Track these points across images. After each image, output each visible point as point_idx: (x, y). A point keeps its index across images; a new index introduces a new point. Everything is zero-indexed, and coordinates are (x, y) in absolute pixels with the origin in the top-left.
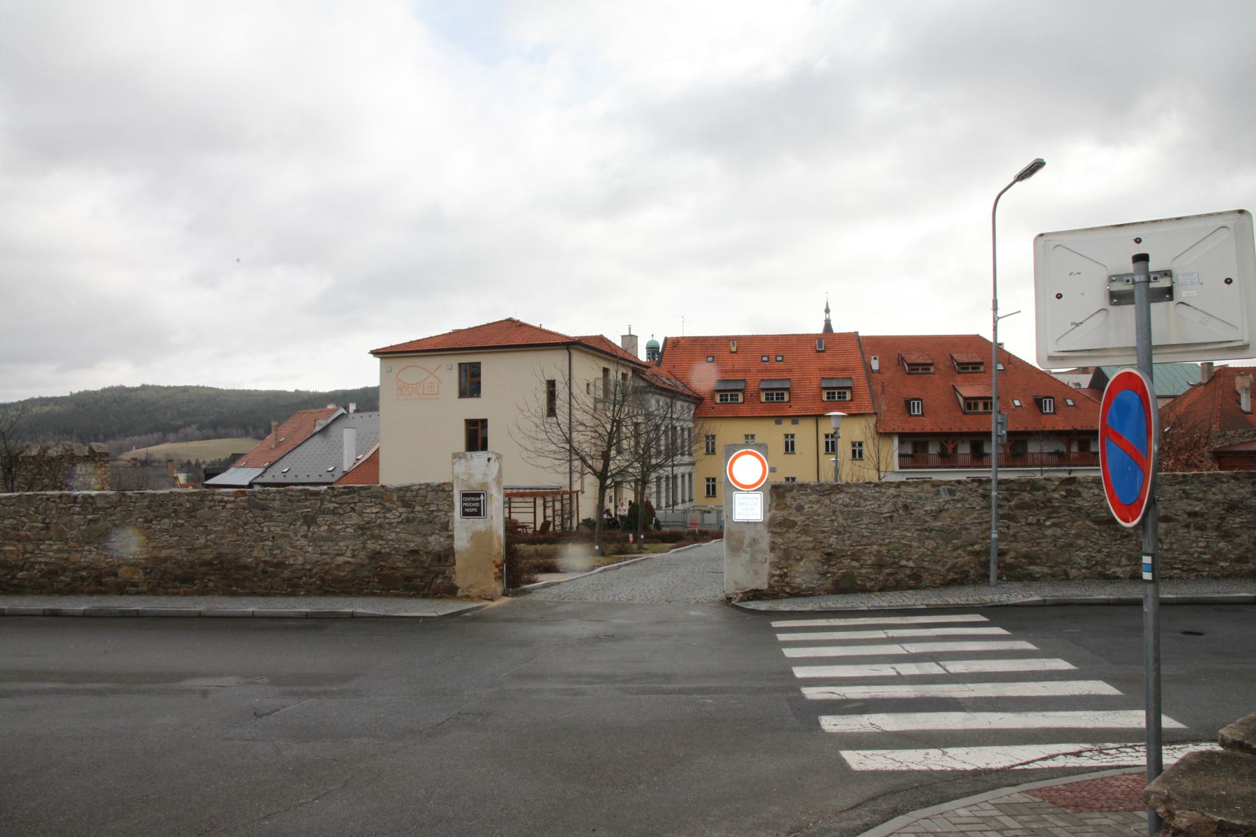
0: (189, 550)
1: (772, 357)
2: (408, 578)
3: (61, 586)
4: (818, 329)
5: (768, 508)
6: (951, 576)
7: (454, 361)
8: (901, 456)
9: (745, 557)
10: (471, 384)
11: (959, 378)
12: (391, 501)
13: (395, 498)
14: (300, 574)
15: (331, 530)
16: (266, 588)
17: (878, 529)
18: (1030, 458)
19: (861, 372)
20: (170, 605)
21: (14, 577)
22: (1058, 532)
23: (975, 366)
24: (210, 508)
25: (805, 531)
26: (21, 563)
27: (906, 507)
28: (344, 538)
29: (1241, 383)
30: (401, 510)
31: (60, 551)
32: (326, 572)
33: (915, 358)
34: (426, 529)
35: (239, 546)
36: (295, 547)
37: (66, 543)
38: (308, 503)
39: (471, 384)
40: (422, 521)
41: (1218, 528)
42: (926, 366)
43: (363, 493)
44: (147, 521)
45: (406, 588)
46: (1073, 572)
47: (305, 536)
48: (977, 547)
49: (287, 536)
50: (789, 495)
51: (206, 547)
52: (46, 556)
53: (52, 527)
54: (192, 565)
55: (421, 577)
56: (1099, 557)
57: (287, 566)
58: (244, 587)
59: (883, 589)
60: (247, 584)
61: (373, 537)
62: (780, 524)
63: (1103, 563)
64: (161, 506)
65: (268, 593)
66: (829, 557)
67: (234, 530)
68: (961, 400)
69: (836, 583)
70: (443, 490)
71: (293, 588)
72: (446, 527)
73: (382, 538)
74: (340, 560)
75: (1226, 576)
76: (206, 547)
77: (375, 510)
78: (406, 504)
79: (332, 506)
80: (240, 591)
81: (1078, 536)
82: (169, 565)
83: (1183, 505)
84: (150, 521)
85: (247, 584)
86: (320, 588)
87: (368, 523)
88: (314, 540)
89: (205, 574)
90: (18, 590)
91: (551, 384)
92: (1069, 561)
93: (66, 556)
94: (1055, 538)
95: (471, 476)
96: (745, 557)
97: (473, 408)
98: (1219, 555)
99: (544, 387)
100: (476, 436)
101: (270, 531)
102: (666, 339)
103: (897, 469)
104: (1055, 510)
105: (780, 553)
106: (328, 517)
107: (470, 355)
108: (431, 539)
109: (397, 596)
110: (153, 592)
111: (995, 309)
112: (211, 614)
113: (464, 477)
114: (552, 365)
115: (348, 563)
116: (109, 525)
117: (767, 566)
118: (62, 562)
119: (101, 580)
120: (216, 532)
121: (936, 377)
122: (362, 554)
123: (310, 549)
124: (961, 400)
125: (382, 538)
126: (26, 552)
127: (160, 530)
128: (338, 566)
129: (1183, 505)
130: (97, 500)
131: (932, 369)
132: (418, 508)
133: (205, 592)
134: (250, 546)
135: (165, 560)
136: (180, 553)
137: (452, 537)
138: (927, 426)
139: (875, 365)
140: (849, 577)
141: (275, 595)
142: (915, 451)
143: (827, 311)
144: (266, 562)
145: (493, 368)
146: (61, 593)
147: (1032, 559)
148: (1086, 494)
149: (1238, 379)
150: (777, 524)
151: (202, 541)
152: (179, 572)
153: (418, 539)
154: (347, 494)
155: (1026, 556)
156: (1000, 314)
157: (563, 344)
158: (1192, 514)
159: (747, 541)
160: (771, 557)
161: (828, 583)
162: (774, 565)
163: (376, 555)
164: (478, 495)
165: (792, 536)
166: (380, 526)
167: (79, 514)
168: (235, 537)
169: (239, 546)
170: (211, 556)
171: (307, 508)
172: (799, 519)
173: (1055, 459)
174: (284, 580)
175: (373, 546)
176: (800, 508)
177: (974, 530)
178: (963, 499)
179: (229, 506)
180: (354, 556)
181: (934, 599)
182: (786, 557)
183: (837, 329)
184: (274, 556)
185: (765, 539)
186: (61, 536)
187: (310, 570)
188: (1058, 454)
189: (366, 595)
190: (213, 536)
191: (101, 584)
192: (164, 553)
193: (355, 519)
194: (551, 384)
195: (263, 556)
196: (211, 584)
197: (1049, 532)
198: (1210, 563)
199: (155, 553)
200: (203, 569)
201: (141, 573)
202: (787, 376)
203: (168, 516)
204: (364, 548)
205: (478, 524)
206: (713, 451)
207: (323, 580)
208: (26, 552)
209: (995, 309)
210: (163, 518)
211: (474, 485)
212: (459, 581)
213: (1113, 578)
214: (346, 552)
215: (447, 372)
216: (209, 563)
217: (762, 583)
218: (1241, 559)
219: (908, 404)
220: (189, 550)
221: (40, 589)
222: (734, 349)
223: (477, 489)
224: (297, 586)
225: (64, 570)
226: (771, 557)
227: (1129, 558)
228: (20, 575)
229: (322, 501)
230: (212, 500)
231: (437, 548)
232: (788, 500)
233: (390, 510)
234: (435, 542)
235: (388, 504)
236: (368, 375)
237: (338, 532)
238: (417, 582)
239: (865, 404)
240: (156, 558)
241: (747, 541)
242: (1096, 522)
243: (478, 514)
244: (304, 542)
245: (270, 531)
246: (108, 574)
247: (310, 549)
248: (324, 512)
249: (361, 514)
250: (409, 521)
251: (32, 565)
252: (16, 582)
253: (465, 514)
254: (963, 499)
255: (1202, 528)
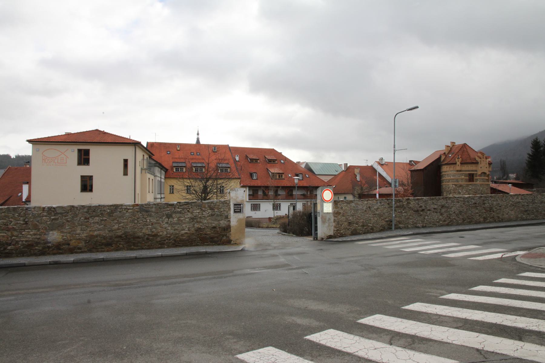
0: (109, 231)
1: (195, 153)
2: (212, 238)
3: (36, 251)
4: (194, 142)
5: (333, 208)
6: (381, 228)
7: (76, 148)
8: (249, 195)
9: (327, 224)
10: (84, 158)
11: (269, 165)
12: (205, 207)
13: (207, 206)
14: (165, 239)
15: (179, 220)
16: (148, 246)
17: (363, 214)
18: (294, 196)
19: (232, 161)
20: (141, 253)
21: (5, 249)
22: (406, 214)
23: (274, 161)
24: (120, 212)
25: (343, 216)
26: (10, 242)
27: (369, 207)
28: (185, 223)
29: (357, 171)
30: (209, 211)
31: (35, 234)
32: (177, 238)
33: (251, 156)
34: (219, 218)
35: (136, 228)
36: (163, 228)
37: (39, 230)
38: (168, 209)
39: (84, 158)
40: (218, 215)
41: (440, 212)
42: (256, 160)
43: (193, 204)
44: (86, 219)
45: (211, 242)
46: (409, 226)
47: (167, 223)
48: (387, 219)
49: (159, 223)
50: (339, 204)
51: (118, 229)
52: (26, 237)
53: (30, 223)
54: (111, 238)
55: (217, 237)
56: (415, 221)
57: (159, 236)
58: (138, 246)
59: (365, 233)
60: (139, 244)
61: (197, 222)
62: (337, 213)
63: (416, 223)
64: (94, 211)
65: (150, 248)
66: (350, 223)
67: (133, 221)
68: (270, 174)
69: (352, 232)
70: (226, 203)
71: (161, 245)
72: (227, 217)
73: (201, 222)
74: (183, 232)
75: (442, 226)
76: (118, 229)
77: (198, 211)
78: (212, 209)
79: (179, 210)
80: (135, 248)
81: (410, 215)
82: (99, 238)
83: (433, 206)
84: (88, 219)
85: (139, 244)
86: (173, 244)
87: (195, 216)
88: (172, 224)
89: (117, 242)
90: (8, 255)
91: (126, 161)
92: (408, 223)
93: (38, 237)
94: (405, 216)
95: (237, 197)
96: (327, 224)
97: (85, 170)
98: (440, 220)
99: (122, 161)
100: (87, 185)
101: (150, 221)
102: (148, 143)
103: (248, 200)
104: (405, 208)
105: (336, 223)
106: (178, 215)
107: (85, 145)
108: (221, 222)
109: (208, 245)
110: (90, 251)
111: (394, 147)
112: (142, 257)
113: (235, 198)
114: (127, 153)
115: (187, 233)
116: (64, 221)
117: (333, 227)
118: (36, 240)
119: (47, 249)
120: (124, 222)
121: (260, 164)
122: (193, 229)
123: (169, 228)
124: (270, 174)
125: (201, 222)
126: (13, 236)
127: (93, 223)
128: (182, 235)
129: (433, 206)
130: (57, 209)
131: (259, 161)
132: (216, 210)
133: (117, 249)
134: (141, 228)
135: (97, 236)
136: (105, 233)
137: (229, 221)
138: (259, 183)
139: (237, 159)
140: (355, 230)
141: (153, 248)
142: (253, 193)
143: (198, 134)
144: (148, 235)
145: (95, 153)
146: (35, 255)
147: (400, 222)
148: (412, 203)
149: (356, 170)
150: (336, 213)
151: (116, 227)
152: (104, 241)
153: (216, 222)
154: (186, 205)
155: (399, 222)
156: (396, 149)
157: (133, 143)
158: (435, 209)
159: (327, 219)
160: (334, 224)
161: (349, 232)
162: (335, 227)
163: (199, 230)
164: (240, 205)
165: (340, 217)
166: (200, 218)
167: (46, 216)
168: (133, 224)
169: (136, 228)
170: (121, 233)
171: (168, 211)
172: (341, 211)
173: (302, 197)
174: (157, 242)
175: (197, 226)
176: (342, 208)
177: (386, 214)
178: (383, 205)
179: (130, 211)
180: (189, 230)
181: (445, 229)
182: (338, 223)
183: (202, 142)
184: (153, 232)
185: (332, 219)
186: (36, 227)
187: (169, 237)
188: (304, 195)
189: (194, 246)
190: (122, 224)
191: (60, 249)
192: (96, 233)
193: (190, 215)
194: (126, 161)
195: (148, 232)
196: (121, 246)
197: (404, 214)
198: (438, 222)
199: (91, 233)
200: (116, 239)
201: (83, 242)
202: (203, 161)
203: (98, 216)
204: (194, 226)
205: (240, 216)
206: (173, 192)
207: (175, 240)
208: (13, 236)
209: (394, 147)
210: (95, 217)
211: (239, 201)
212: (232, 238)
213: (418, 227)
214: (186, 228)
215: (72, 153)
216: (120, 237)
217: (332, 233)
218: (445, 221)
219: (251, 175)
220: (109, 231)
221: (22, 254)
222: (178, 149)
223: (239, 202)
224: (164, 244)
225: (39, 243)
226: (334, 224)
227: (422, 221)
228: (9, 248)
229: (175, 208)
230: (122, 208)
231: (224, 225)
232: (339, 205)
233: (204, 211)
234: (223, 223)
235: (203, 209)
236: (27, 150)
237: (182, 221)
238: (216, 239)
239: (237, 175)
240: (92, 235)
241: (327, 219)
242: (414, 211)
243: (240, 212)
244: (166, 225)
245: (150, 221)
246: (64, 244)
247: (169, 228)
248: (175, 213)
249: (192, 213)
250: (212, 215)
251: (17, 242)
252: (7, 251)
253: (235, 212)
254: (383, 205)
255: (437, 213)
